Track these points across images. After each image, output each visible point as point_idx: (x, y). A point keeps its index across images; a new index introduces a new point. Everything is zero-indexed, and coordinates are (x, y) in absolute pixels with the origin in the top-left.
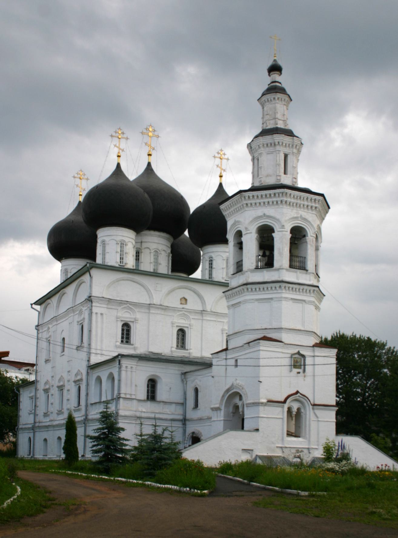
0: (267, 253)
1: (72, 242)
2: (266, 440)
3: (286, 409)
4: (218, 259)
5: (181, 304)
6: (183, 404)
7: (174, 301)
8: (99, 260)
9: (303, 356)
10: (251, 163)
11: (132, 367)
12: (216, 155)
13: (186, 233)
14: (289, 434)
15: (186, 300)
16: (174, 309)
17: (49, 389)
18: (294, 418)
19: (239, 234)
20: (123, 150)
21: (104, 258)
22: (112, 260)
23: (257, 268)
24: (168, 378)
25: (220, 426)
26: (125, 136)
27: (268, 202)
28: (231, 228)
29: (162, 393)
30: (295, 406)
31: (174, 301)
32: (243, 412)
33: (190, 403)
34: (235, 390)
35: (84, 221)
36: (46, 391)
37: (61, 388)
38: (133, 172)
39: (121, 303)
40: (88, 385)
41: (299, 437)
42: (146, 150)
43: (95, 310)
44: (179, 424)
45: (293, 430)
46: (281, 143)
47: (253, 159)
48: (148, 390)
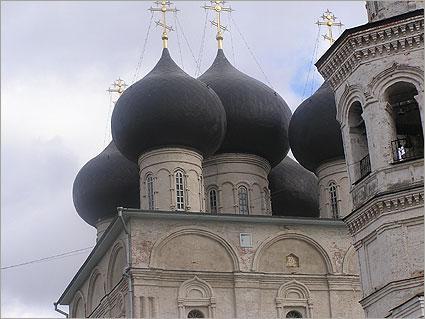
1: (109, 192)
8: (144, 204)
12: (321, 20)
13: (290, 154)
20: (171, 29)
21: (151, 203)
22: (165, 201)
23: (397, 162)
26: (172, 7)
35: (123, 153)
38: (193, 66)
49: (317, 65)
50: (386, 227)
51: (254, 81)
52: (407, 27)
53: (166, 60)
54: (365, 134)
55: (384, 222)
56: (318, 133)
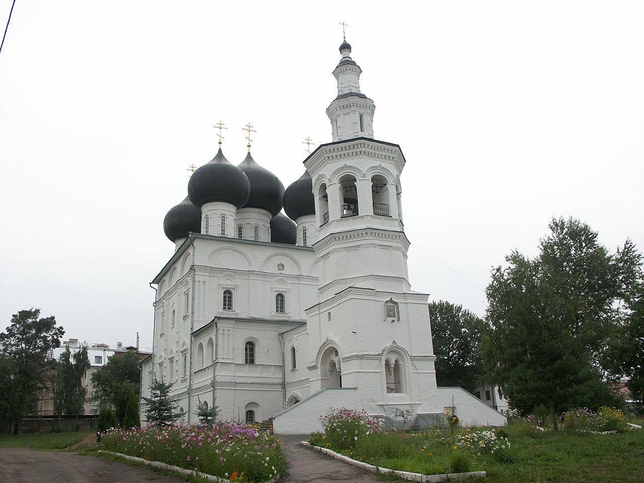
0: (352, 207)
1: (182, 225)
2: (365, 396)
3: (383, 363)
4: (310, 228)
5: (279, 270)
6: (282, 367)
7: (272, 268)
8: (203, 232)
9: (396, 303)
10: (332, 136)
11: (229, 330)
13: (283, 211)
14: (390, 390)
15: (283, 266)
16: (272, 275)
17: (162, 362)
18: (392, 373)
19: (324, 187)
21: (207, 231)
22: (215, 231)
24: (265, 340)
25: (317, 386)
27: (348, 154)
28: (315, 183)
29: (260, 356)
30: (393, 359)
31: (272, 268)
32: (340, 369)
33: (289, 366)
34: (330, 345)
36: (161, 364)
37: (171, 360)
38: (235, 159)
39: (222, 270)
40: (191, 354)
41: (401, 393)
42: (247, 142)
43: (197, 278)
44: (280, 388)
45: (393, 386)
46: (355, 104)
47: (332, 123)
48: (246, 354)
49: (304, 162)
50: (335, 250)
51: (266, 171)
52: (354, 146)
53: (220, 154)
54: (327, 201)
55: (335, 248)
56: (301, 200)
